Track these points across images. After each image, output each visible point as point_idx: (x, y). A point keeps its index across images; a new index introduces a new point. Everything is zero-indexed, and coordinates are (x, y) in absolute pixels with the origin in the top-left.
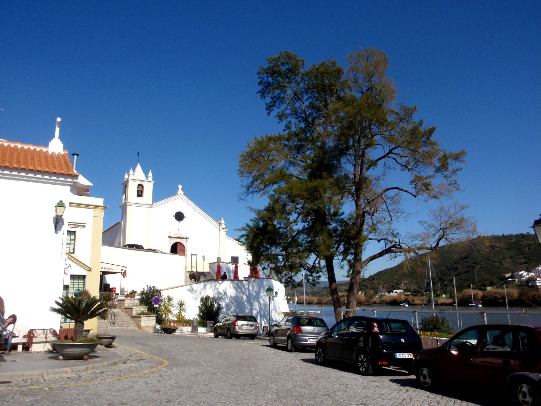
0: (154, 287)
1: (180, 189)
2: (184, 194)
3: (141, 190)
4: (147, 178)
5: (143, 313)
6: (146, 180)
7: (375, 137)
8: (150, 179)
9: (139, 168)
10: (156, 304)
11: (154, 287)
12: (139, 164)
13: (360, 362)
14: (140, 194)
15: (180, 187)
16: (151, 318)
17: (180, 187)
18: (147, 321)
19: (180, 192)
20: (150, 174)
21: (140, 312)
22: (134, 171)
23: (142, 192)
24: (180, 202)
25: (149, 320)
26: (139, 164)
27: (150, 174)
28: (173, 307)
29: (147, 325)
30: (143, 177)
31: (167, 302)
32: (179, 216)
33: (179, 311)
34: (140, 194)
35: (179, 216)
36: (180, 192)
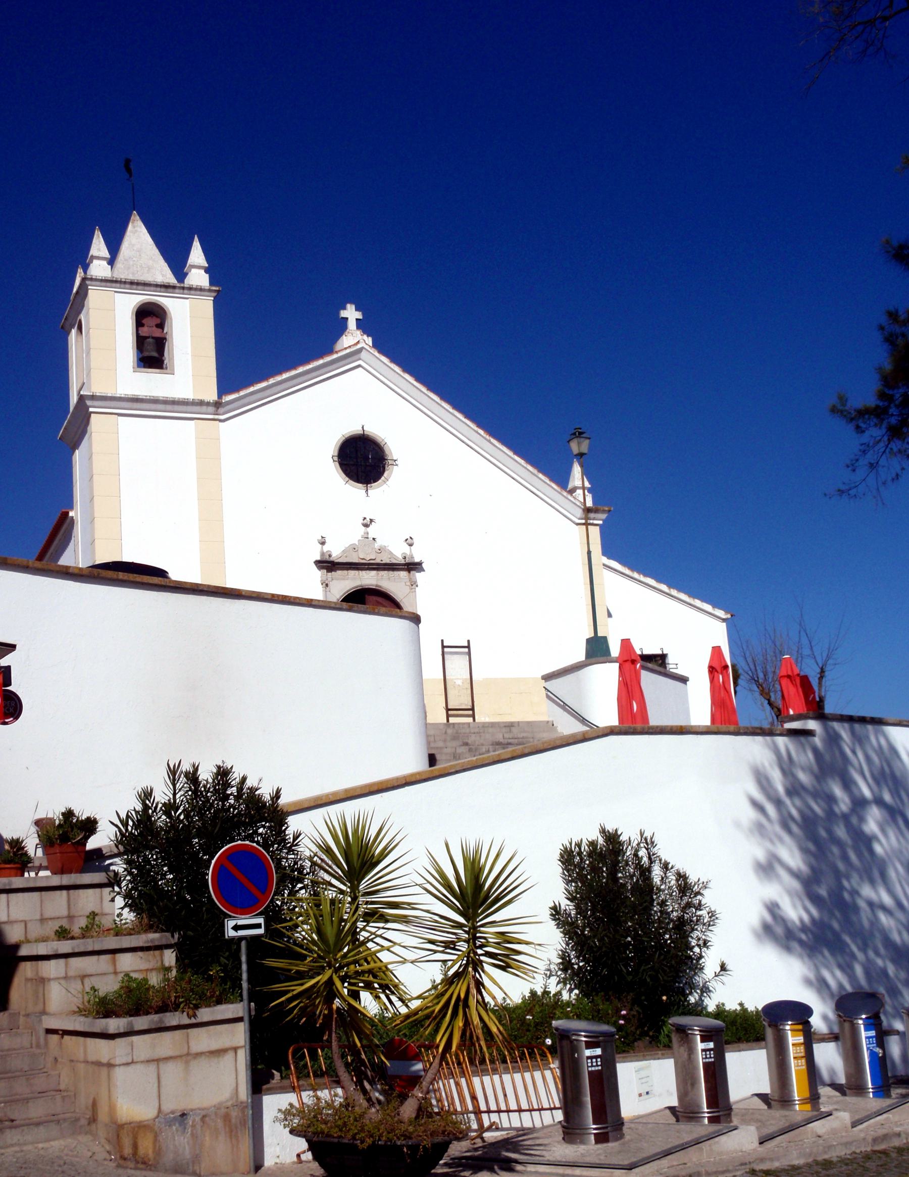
0: (223, 774)
1: (352, 325)
2: (375, 345)
3: (157, 333)
4: (178, 266)
5: (134, 1002)
6: (171, 279)
7: (141, 1151)
8: (198, 277)
9: (138, 238)
10: (245, 908)
11: (223, 774)
12: (196, 238)
13: (37, 874)
14: (152, 352)
15: (351, 314)
16: (202, 1040)
17: (351, 314)
18: (171, 1071)
19: (353, 338)
20: (197, 255)
21: (109, 986)
22: (114, 246)
23: (160, 343)
24: (363, 387)
25: (188, 1057)
26: (196, 238)
27: (197, 255)
28: (395, 933)
29: (171, 1105)
30: (163, 273)
31: (335, 887)
32: (362, 459)
33: (455, 961)
34: (152, 352)
35: (362, 459)
36: (353, 338)
